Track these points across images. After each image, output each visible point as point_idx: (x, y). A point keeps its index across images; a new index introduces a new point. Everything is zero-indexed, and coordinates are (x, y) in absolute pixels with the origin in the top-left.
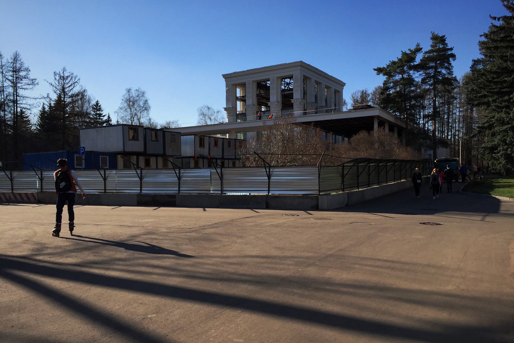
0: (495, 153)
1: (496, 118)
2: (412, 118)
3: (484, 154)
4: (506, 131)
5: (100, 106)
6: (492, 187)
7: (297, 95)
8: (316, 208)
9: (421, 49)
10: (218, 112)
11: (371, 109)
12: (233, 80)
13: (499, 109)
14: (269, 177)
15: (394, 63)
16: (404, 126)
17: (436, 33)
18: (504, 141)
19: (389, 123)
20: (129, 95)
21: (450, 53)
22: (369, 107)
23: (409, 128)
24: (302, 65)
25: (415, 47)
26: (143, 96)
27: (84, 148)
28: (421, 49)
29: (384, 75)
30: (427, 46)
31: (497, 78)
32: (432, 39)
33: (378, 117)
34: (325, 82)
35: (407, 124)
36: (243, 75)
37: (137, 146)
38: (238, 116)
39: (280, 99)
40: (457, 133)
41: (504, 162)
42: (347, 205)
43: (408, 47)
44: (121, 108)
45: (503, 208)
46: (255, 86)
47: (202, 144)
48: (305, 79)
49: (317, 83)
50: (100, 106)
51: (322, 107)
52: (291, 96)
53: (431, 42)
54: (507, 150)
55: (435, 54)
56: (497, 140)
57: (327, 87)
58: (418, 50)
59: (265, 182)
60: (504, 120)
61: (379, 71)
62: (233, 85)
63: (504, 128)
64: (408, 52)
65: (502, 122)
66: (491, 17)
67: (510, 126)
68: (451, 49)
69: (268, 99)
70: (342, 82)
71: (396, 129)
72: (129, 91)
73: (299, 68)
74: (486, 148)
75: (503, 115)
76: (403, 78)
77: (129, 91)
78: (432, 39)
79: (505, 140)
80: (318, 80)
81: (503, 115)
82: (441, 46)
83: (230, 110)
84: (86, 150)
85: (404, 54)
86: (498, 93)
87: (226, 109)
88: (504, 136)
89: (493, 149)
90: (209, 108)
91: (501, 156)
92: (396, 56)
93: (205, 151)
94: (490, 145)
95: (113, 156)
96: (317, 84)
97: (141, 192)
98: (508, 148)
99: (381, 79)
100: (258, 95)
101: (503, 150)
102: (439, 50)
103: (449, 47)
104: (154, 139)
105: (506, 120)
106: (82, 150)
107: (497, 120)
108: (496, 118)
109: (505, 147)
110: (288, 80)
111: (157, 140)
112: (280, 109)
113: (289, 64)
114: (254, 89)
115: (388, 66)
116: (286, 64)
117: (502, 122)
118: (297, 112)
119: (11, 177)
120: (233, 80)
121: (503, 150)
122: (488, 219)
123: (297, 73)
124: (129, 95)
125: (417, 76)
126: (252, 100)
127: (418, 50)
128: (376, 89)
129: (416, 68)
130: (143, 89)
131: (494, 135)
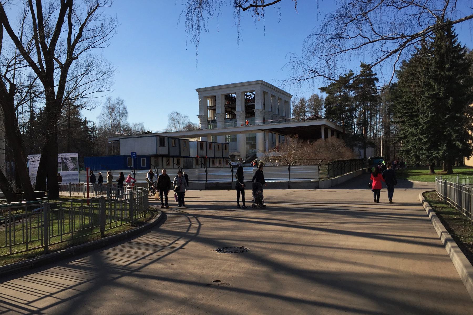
0: (409, 154)
1: (409, 132)
2: (349, 126)
3: (402, 155)
4: (415, 140)
6: (408, 176)
7: (258, 106)
8: (318, 187)
10: (185, 117)
11: (319, 120)
13: (411, 126)
14: (289, 171)
16: (342, 131)
18: (415, 147)
19: (337, 131)
20: (109, 103)
21: (374, 77)
22: (321, 118)
23: (346, 132)
24: (262, 83)
27: (135, 153)
28: (354, 74)
30: (357, 71)
31: (409, 106)
32: (361, 66)
33: (325, 126)
34: (277, 95)
35: (344, 130)
37: (164, 151)
38: (209, 122)
39: (244, 109)
40: (378, 133)
41: (414, 160)
42: (332, 186)
44: (103, 114)
45: (414, 186)
46: (223, 97)
47: (202, 148)
48: (264, 93)
49: (272, 96)
51: (283, 117)
52: (253, 107)
53: (360, 69)
54: (416, 152)
56: (410, 146)
57: (279, 99)
60: (414, 134)
62: (205, 97)
63: (414, 138)
65: (413, 135)
67: (418, 137)
68: (375, 74)
69: (235, 109)
71: (335, 133)
72: (109, 99)
73: (260, 85)
74: (403, 151)
75: (413, 130)
77: (109, 99)
78: (361, 66)
79: (415, 146)
80: (274, 94)
81: (413, 130)
83: (202, 117)
86: (409, 116)
87: (199, 117)
88: (414, 143)
89: (408, 151)
91: (413, 156)
93: (203, 153)
94: (405, 149)
95: (149, 157)
96: (272, 97)
98: (417, 151)
100: (225, 105)
101: (414, 152)
102: (367, 75)
103: (374, 73)
104: (174, 145)
105: (415, 133)
107: (410, 133)
108: (409, 132)
109: (415, 150)
110: (249, 94)
111: (175, 146)
112: (244, 117)
113: (251, 82)
114: (224, 102)
115: (329, 86)
116: (249, 82)
117: (413, 135)
118: (259, 121)
121: (414, 152)
122: (407, 190)
123: (258, 90)
124: (109, 103)
125: (352, 94)
126: (220, 109)
128: (312, 96)
129: (350, 88)
130: (122, 98)
131: (408, 142)
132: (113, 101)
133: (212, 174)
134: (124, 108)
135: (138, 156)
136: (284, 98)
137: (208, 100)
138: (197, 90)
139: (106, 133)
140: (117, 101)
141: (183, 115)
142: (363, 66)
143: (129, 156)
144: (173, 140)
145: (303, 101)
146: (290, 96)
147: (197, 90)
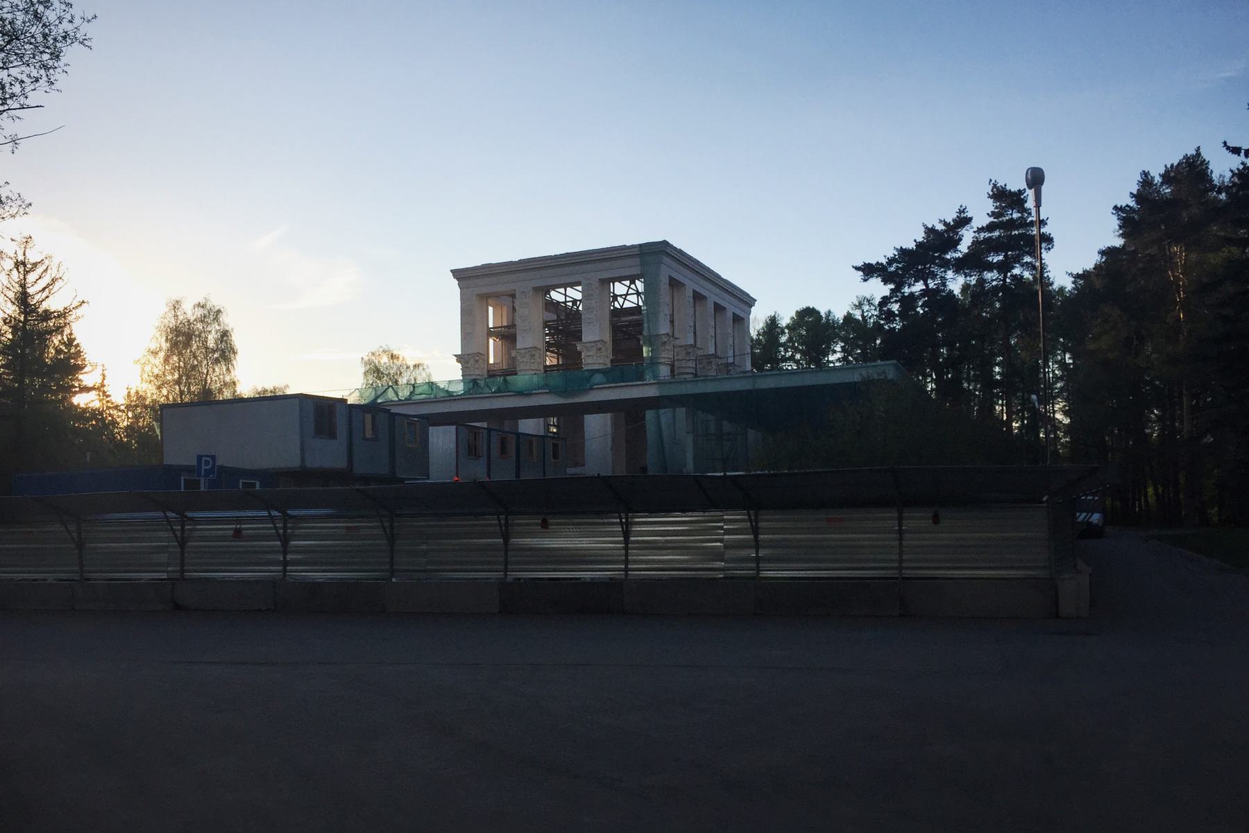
5: (77, 345)
9: (971, 219)
12: (478, 284)
15: (903, 252)
17: (1001, 184)
25: (955, 216)
26: (216, 319)
27: (213, 458)
28: (971, 219)
29: (885, 281)
30: (982, 212)
34: (713, 296)
36: (616, 258)
39: (607, 336)
43: (940, 215)
50: (77, 345)
53: (990, 206)
55: (996, 233)
58: (963, 221)
59: (517, 563)
61: (869, 270)
64: (940, 227)
66: (1228, 148)
70: (748, 295)
72: (176, 306)
76: (926, 292)
77: (176, 306)
82: (1016, 215)
84: (219, 463)
85: (930, 231)
87: (460, 358)
90: (392, 356)
92: (911, 237)
97: (627, 575)
99: (878, 289)
102: (1012, 224)
104: (369, 434)
106: (207, 463)
115: (891, 261)
116: (624, 248)
119: (183, 538)
120: (478, 284)
127: (963, 221)
130: (215, 302)
132: (189, 312)
133: (528, 541)
134: (225, 335)
135: (222, 468)
136: (731, 307)
137: (491, 309)
138: (459, 274)
139: (162, 411)
140: (199, 312)
141: (411, 364)
142: (1000, 194)
143: (189, 469)
144: (368, 417)
145: (772, 323)
146: (749, 302)
147: (459, 274)
